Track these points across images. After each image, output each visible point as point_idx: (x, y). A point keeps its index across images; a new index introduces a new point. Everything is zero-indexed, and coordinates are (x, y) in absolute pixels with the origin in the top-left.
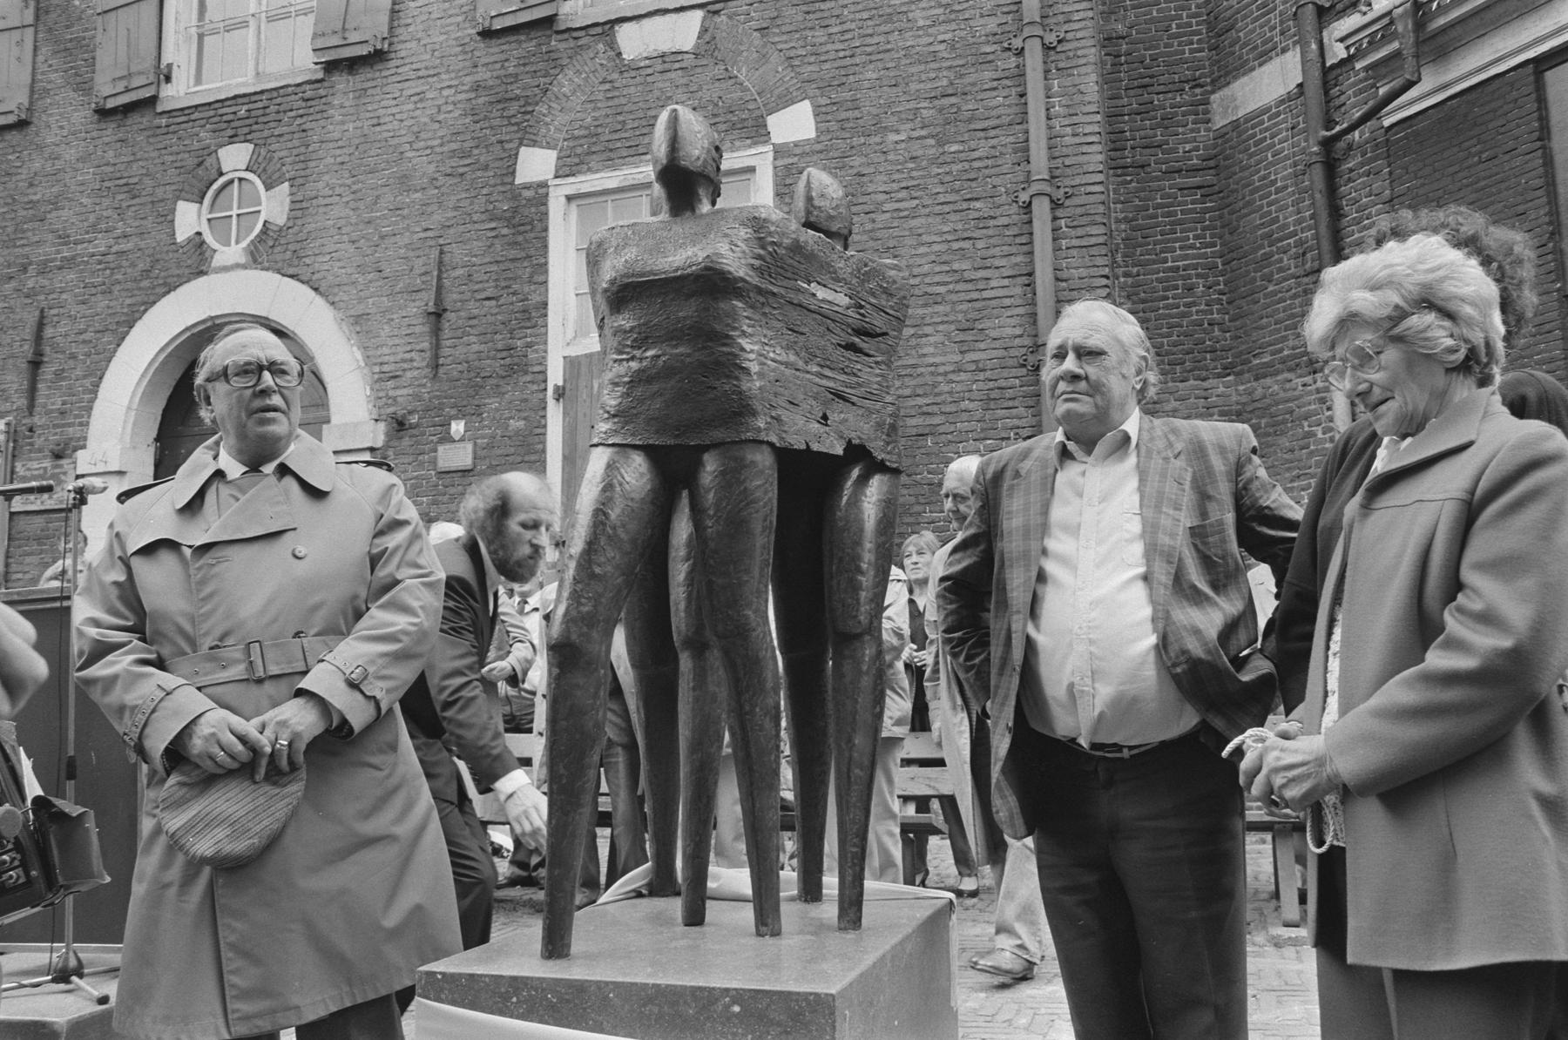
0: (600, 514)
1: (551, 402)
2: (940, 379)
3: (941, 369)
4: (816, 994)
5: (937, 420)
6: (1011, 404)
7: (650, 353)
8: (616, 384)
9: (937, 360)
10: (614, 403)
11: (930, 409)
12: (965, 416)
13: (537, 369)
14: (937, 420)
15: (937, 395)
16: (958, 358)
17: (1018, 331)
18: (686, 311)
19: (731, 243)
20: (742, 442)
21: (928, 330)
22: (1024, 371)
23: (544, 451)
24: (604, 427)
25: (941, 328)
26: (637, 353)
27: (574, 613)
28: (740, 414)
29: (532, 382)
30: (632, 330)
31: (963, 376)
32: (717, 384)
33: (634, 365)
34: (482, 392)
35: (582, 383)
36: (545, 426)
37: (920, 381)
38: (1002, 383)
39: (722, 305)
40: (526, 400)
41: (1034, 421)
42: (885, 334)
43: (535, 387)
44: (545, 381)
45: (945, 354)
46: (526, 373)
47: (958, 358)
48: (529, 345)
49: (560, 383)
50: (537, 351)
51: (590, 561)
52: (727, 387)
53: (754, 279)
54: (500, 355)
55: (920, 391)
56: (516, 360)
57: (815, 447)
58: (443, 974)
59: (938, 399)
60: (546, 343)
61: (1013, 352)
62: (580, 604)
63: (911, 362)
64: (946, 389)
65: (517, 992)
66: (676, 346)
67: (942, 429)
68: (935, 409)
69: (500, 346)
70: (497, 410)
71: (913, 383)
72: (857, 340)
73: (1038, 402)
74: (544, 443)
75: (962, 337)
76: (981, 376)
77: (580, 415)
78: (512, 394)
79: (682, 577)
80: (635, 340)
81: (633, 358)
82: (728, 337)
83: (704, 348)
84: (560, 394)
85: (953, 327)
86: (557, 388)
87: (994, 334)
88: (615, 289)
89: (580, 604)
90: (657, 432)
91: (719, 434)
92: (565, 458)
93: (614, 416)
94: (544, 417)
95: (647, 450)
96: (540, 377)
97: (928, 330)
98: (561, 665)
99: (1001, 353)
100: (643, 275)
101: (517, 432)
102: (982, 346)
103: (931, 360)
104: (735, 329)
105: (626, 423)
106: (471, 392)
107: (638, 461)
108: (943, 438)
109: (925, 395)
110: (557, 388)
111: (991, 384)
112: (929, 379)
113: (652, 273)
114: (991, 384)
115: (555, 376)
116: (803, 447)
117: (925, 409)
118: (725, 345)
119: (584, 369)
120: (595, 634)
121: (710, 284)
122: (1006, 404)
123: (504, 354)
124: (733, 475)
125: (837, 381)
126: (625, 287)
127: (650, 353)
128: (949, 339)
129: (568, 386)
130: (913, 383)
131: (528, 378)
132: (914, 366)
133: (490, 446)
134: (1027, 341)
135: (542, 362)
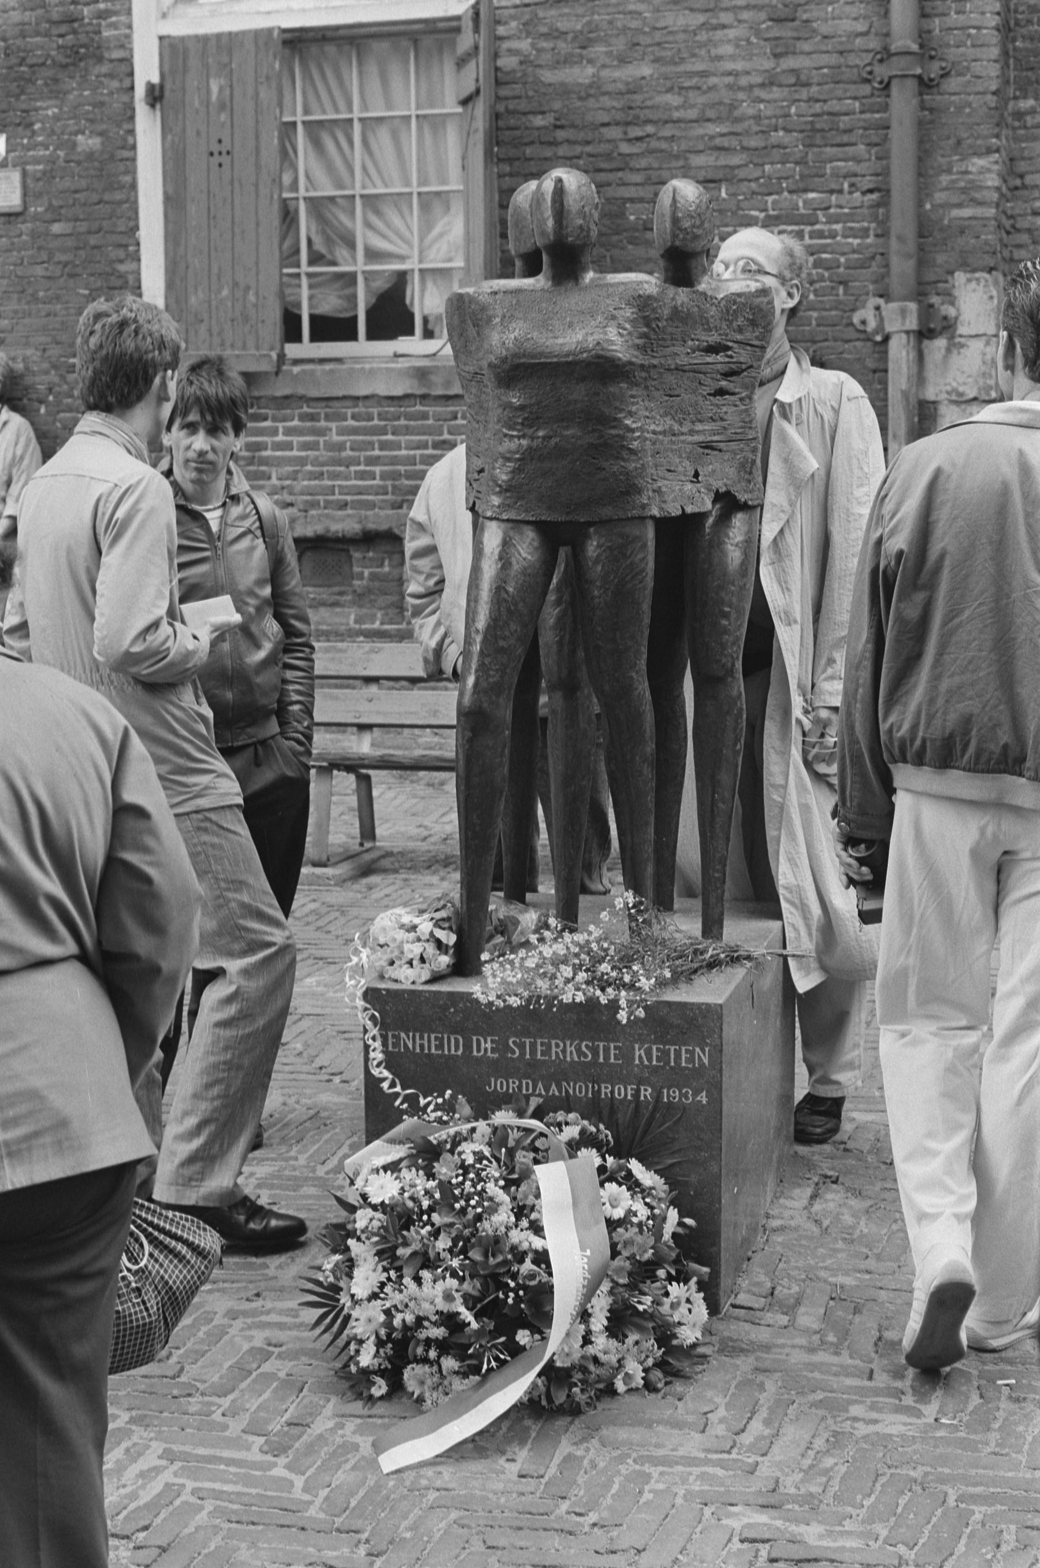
0: (499, 590)
1: (141, 109)
2: (741, 96)
3: (744, 81)
4: (707, 1004)
5: (736, 160)
6: (845, 138)
7: (541, 433)
8: (509, 460)
9: (739, 66)
10: (504, 477)
11: (725, 142)
12: (776, 154)
13: (117, 54)
14: (736, 160)
15: (738, 120)
16: (768, 64)
17: (861, 27)
18: (578, 393)
19: (619, 326)
20: (628, 519)
21: (725, 18)
22: (866, 89)
23: (134, 186)
24: (496, 500)
25: (745, 15)
26: (529, 432)
27: (484, 684)
28: (628, 493)
29: (111, 76)
30: (522, 408)
31: (776, 93)
32: (605, 465)
33: (524, 442)
34: (30, 89)
35: (193, 81)
36: (134, 147)
37: (713, 97)
38: (834, 106)
39: (611, 389)
40: (102, 104)
41: (878, 166)
42: (751, 367)
43: (115, 84)
44: (131, 74)
45: (750, 57)
46: (100, 59)
47: (768, 64)
48: (102, 15)
49: (156, 79)
50: (114, 26)
51: (496, 637)
52: (615, 469)
53: (639, 359)
54: (55, 31)
55: (711, 114)
56: (83, 38)
57: (689, 510)
58: (387, 990)
59: (739, 128)
60: (129, 12)
61: (853, 60)
62: (489, 676)
63: (699, 67)
64: (751, 112)
65: (454, 1004)
66: (567, 428)
67: (741, 174)
68: (734, 142)
69: (55, 16)
70: (57, 118)
71: (701, 100)
72: (724, 383)
73: (886, 138)
74: (133, 172)
75: (775, 32)
76: (804, 94)
77: (190, 133)
78: (76, 92)
79: (552, 621)
80: (525, 419)
81: (524, 436)
82: (616, 419)
83: (594, 430)
84: (155, 96)
85: (763, 16)
86: (151, 88)
87: (825, 29)
88: (506, 367)
89: (489, 676)
90: (549, 508)
91: (607, 512)
92: (168, 199)
93: (507, 490)
94: (132, 132)
95: (540, 526)
96: (124, 68)
97: (725, 18)
98: (473, 730)
99: (834, 59)
100: (533, 357)
101: (90, 156)
102: (806, 47)
103: (729, 66)
104: (622, 410)
105: (519, 498)
106: (13, 87)
107: (530, 534)
108: (744, 187)
109: (718, 120)
110: (151, 88)
111: (818, 107)
112: (726, 97)
113: (542, 354)
114: (818, 107)
115: (147, 69)
116: (679, 512)
117: (718, 141)
118: (614, 427)
119: (194, 62)
120: (501, 700)
121: (600, 370)
122: (838, 140)
123: (63, 28)
124: (620, 553)
125: (705, 431)
126: (517, 367)
127: (541, 433)
128: (758, 33)
129: (168, 86)
130: (701, 100)
131: (105, 69)
132: (704, 74)
133: (48, 176)
134: (874, 44)
135: (125, 43)
